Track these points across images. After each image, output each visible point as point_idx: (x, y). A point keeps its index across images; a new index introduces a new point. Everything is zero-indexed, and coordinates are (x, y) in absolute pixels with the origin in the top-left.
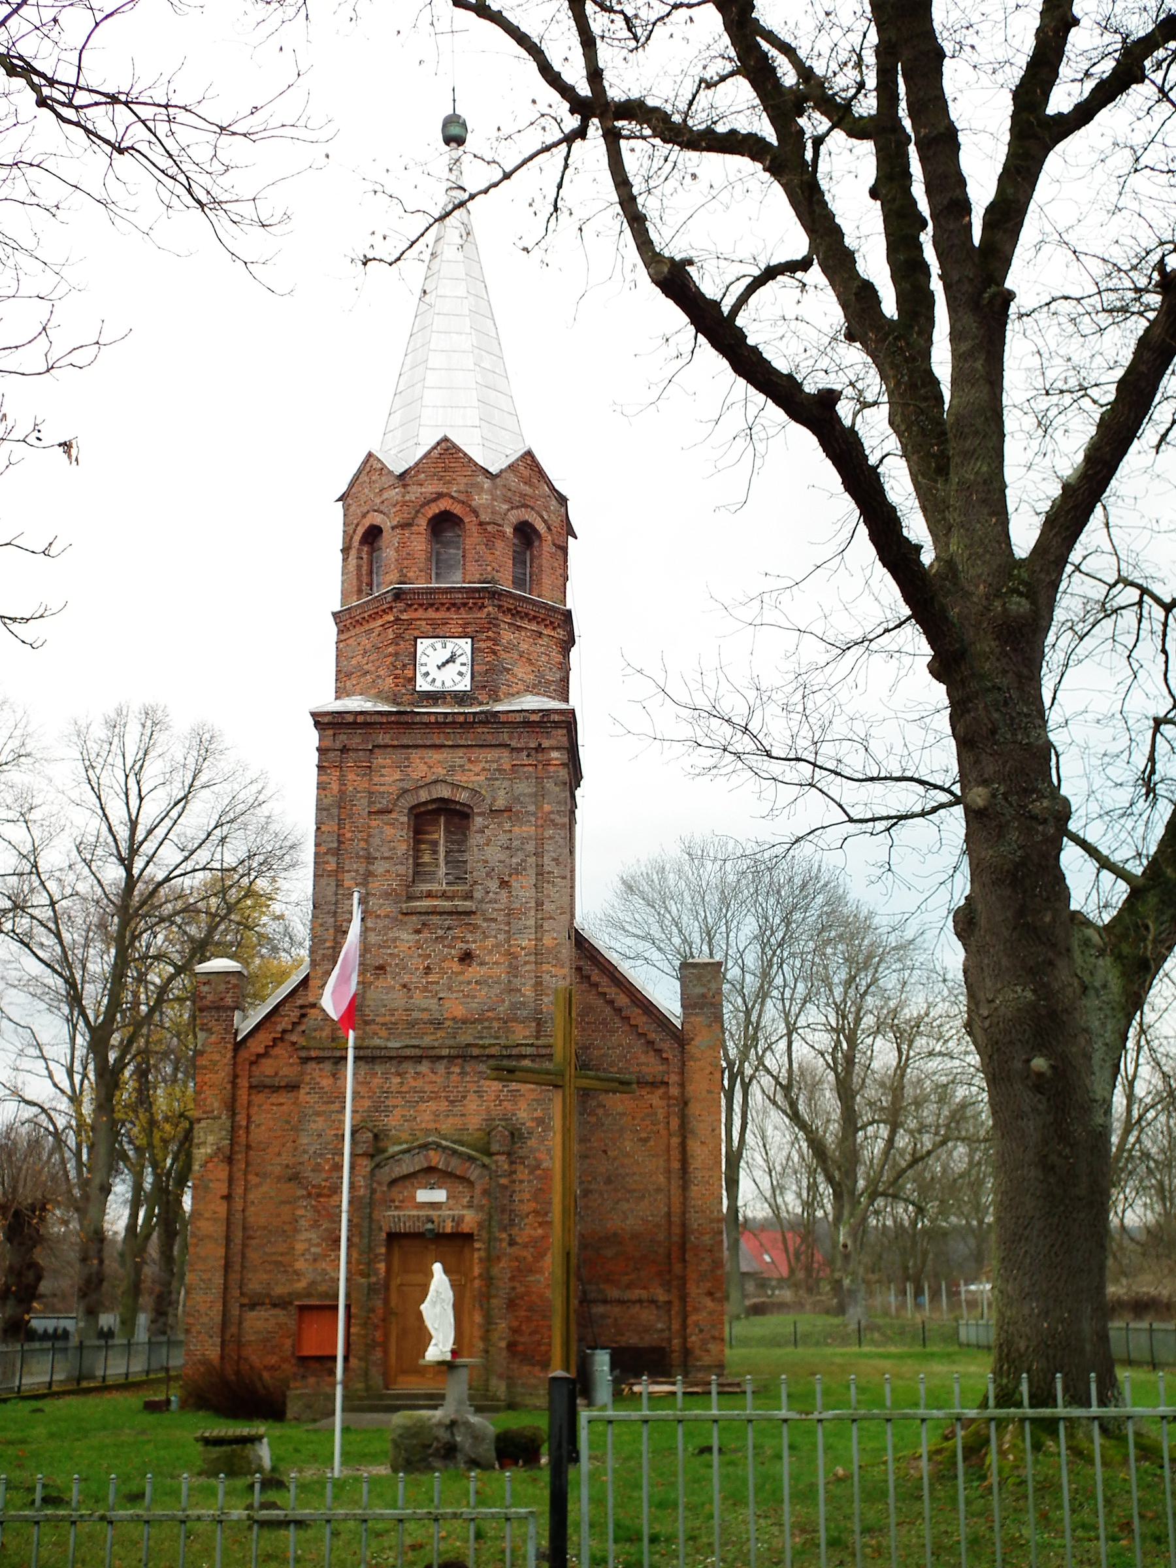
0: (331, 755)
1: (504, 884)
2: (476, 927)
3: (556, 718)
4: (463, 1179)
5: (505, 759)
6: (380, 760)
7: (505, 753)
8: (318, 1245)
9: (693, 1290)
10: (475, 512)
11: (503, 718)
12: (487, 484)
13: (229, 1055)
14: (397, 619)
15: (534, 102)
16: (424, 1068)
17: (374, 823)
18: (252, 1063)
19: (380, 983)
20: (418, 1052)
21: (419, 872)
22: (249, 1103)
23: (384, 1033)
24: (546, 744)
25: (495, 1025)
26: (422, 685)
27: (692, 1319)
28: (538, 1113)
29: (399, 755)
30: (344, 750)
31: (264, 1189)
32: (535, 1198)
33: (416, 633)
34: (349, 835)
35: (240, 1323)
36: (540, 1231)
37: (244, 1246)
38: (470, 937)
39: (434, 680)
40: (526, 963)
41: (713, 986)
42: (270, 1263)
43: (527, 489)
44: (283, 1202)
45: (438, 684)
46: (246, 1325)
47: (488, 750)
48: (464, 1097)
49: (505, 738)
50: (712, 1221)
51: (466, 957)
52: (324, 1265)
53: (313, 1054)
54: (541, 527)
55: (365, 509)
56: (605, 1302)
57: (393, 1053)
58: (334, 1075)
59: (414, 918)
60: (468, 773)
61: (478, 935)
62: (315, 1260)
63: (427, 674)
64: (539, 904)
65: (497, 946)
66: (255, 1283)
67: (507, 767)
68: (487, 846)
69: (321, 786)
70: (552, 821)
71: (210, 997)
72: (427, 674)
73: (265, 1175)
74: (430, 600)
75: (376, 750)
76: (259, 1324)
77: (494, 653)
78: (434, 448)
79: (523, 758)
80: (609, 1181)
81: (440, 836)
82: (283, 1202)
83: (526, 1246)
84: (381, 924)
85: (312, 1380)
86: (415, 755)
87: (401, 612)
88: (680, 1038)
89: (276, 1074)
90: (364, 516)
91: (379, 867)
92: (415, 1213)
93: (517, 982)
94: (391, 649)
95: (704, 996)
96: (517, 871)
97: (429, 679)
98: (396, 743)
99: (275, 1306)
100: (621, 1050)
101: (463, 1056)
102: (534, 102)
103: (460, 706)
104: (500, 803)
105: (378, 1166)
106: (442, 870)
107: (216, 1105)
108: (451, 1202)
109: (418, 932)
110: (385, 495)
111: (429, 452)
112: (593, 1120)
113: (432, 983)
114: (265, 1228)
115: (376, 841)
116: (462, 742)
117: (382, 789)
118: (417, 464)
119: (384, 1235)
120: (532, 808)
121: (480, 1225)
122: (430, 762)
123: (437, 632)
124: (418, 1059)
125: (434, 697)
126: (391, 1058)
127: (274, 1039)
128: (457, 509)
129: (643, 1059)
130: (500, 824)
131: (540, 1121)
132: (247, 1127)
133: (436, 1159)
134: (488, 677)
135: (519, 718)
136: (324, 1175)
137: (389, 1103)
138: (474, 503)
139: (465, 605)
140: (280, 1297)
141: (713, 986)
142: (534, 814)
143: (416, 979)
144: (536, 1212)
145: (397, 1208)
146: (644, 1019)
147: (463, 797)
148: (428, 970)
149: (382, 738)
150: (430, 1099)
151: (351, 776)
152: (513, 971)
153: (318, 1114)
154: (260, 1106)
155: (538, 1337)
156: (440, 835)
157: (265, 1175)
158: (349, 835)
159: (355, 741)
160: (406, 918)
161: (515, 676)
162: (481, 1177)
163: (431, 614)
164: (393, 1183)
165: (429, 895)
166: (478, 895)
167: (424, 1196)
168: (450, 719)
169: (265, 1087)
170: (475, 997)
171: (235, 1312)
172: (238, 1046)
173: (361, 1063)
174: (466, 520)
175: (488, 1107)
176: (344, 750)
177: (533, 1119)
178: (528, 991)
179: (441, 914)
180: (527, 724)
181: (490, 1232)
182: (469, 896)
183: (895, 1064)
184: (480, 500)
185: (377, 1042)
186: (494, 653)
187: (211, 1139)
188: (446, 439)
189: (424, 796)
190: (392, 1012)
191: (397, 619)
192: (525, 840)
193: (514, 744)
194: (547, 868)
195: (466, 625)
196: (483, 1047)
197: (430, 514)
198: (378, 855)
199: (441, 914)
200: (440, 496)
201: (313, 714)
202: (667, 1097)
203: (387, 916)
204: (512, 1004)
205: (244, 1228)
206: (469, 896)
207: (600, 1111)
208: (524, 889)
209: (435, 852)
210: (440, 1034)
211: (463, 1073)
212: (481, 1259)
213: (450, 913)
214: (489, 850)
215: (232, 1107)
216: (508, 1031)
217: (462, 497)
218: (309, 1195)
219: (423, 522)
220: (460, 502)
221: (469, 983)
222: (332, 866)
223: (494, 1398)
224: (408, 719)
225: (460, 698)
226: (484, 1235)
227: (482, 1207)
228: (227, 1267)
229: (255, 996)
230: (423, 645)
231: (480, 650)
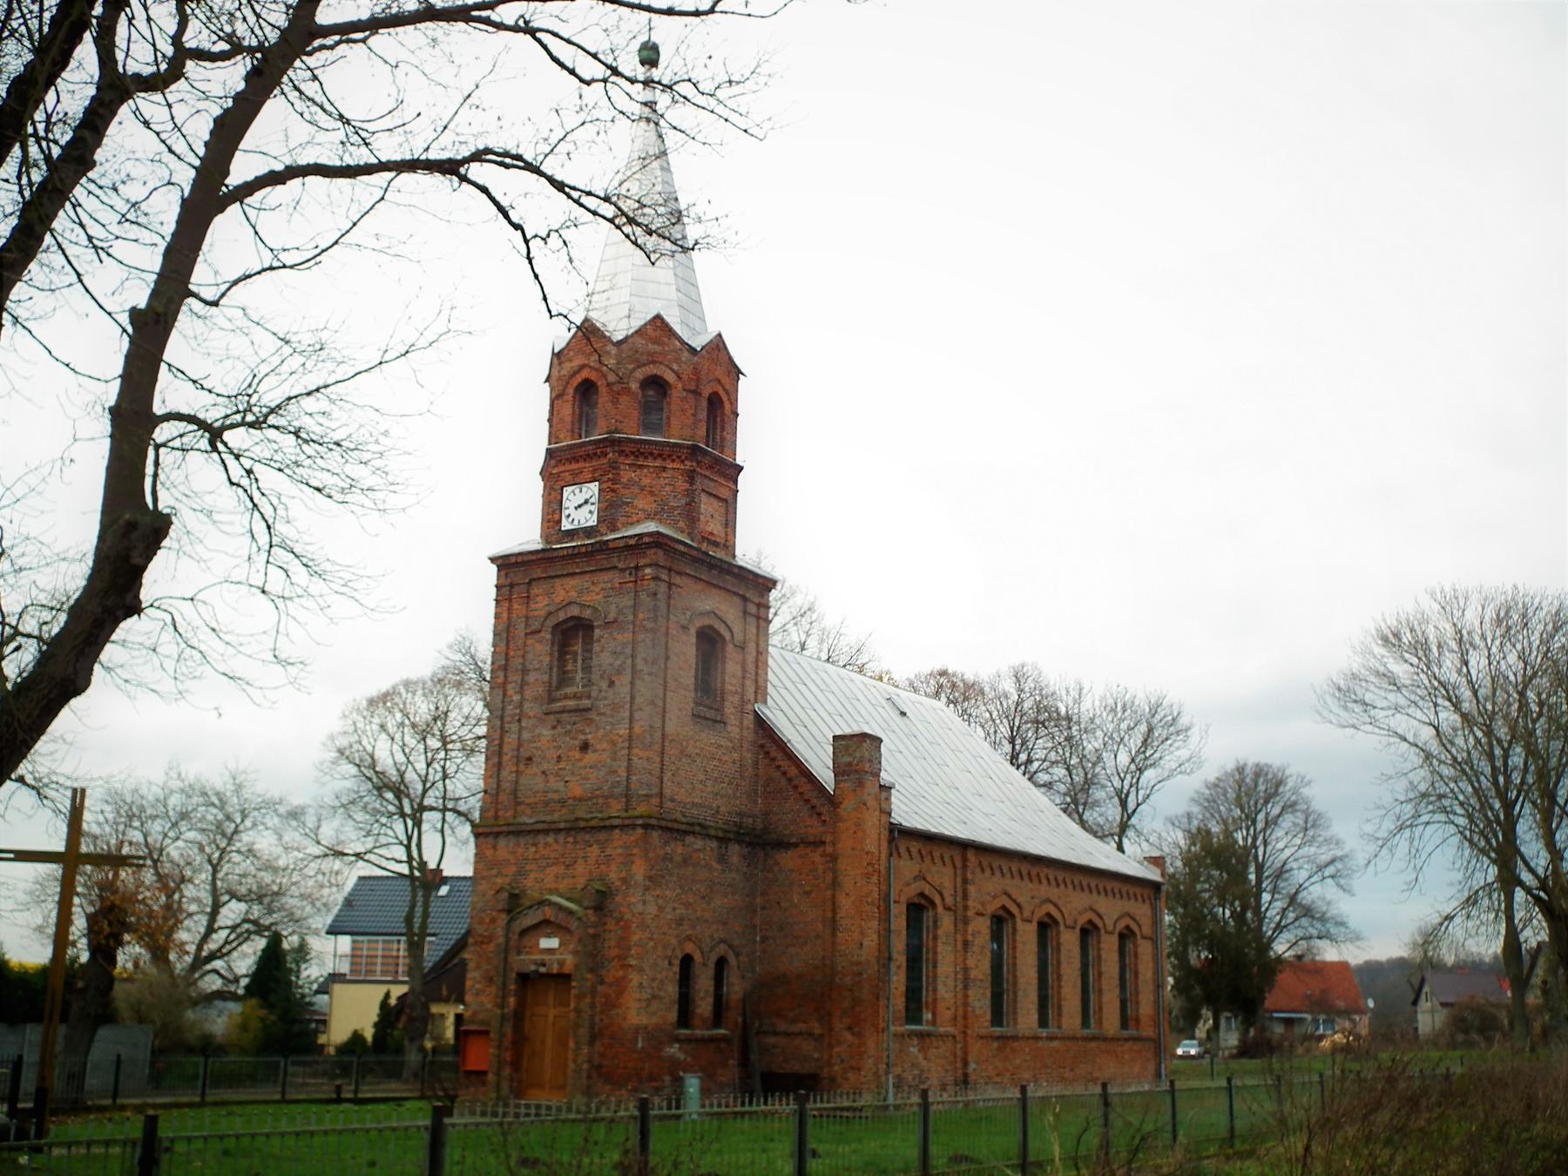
1: (611, 684)
2: (592, 720)
3: (646, 540)
4: (567, 930)
5: (616, 578)
9: (838, 1025)
11: (611, 545)
16: (550, 839)
19: (528, 771)
21: (564, 679)
23: (528, 812)
26: (566, 525)
28: (623, 874)
29: (546, 586)
30: (512, 586)
41: (858, 755)
43: (657, 348)
50: (853, 964)
51: (585, 747)
54: (670, 377)
56: (775, 1034)
64: (633, 698)
69: (497, 616)
80: (781, 929)
83: (610, 985)
84: (531, 722)
88: (833, 801)
91: (531, 677)
95: (850, 764)
100: (791, 817)
109: (554, 728)
112: (770, 875)
121: (576, 966)
124: (546, 832)
125: (571, 534)
129: (808, 823)
131: (624, 881)
134: (610, 511)
135: (621, 543)
144: (619, 957)
146: (809, 787)
147: (587, 614)
151: (516, 606)
156: (578, 648)
161: (634, 507)
163: (568, 467)
165: (566, 697)
173: (481, 839)
180: (628, 547)
183: (1118, 819)
186: (613, 491)
189: (562, 616)
193: (620, 565)
195: (595, 471)
201: (493, 560)
202: (824, 855)
207: (776, 869)
209: (575, 661)
210: (565, 810)
213: (575, 711)
216: (608, 806)
222: (501, 680)
225: (588, 532)
229: (239, 788)
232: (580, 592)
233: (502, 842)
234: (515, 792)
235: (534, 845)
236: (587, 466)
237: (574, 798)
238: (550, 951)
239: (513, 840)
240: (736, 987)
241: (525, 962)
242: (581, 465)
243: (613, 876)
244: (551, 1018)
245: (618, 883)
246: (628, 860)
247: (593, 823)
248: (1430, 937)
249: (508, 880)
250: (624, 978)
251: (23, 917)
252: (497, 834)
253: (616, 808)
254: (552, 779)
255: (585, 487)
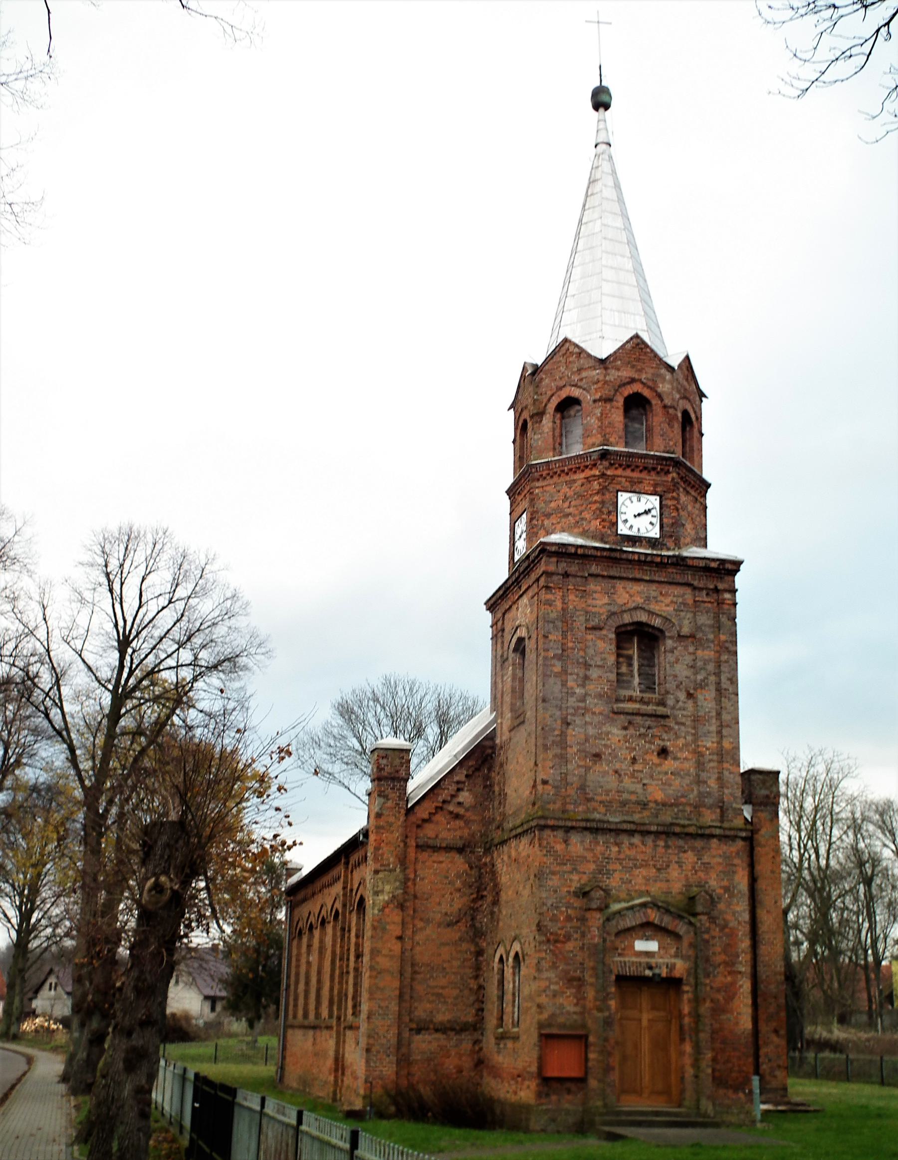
0: (555, 578)
1: (690, 696)
2: (671, 729)
4: (677, 936)
6: (592, 586)
7: (688, 591)
8: (557, 983)
10: (660, 396)
11: (690, 562)
12: (668, 377)
13: (402, 818)
14: (603, 475)
15: (601, 100)
16: (636, 840)
17: (589, 637)
18: (418, 826)
19: (597, 768)
20: (633, 827)
22: (416, 859)
23: (602, 809)
24: (721, 586)
25: (688, 809)
26: (623, 529)
27: (763, 1051)
28: (725, 883)
31: (428, 931)
32: (725, 951)
33: (618, 487)
34: (570, 645)
35: (409, 1045)
36: (729, 979)
37: (413, 979)
38: (665, 736)
39: (631, 527)
40: (710, 761)
42: (433, 994)
44: (443, 944)
45: (635, 530)
46: (413, 1046)
47: (674, 587)
48: (668, 866)
49: (689, 578)
51: (663, 752)
52: (561, 1000)
53: (550, 822)
55: (562, 383)
57: (613, 827)
58: (565, 841)
59: (622, 717)
60: (662, 604)
61: (671, 735)
62: (554, 996)
63: (626, 521)
64: (719, 714)
65: (686, 745)
66: (421, 1011)
67: (690, 602)
68: (676, 663)
70: (727, 648)
71: (388, 769)
72: (626, 521)
73: (428, 921)
74: (628, 462)
75: (590, 579)
76: (424, 1046)
77: (677, 509)
78: (627, 342)
79: (703, 596)
81: (634, 652)
82: (443, 944)
83: (718, 990)
84: (596, 719)
85: (554, 1098)
86: (620, 585)
87: (607, 469)
89: (437, 836)
90: (560, 388)
91: (594, 673)
92: (634, 959)
93: (704, 775)
94: (596, 498)
95: (767, 797)
96: (702, 685)
97: (628, 525)
98: (605, 573)
99: (437, 1030)
101: (667, 833)
102: (601, 100)
103: (653, 548)
104: (686, 630)
105: (608, 919)
106: (637, 680)
107: (391, 860)
108: (662, 952)
109: (625, 728)
110: (584, 374)
111: (624, 345)
113: (638, 771)
114: (428, 965)
115: (591, 651)
116: (657, 578)
117: (594, 610)
118: (615, 352)
119: (613, 977)
120: (711, 636)
122: (632, 591)
123: (635, 488)
124: (631, 833)
126: (610, 830)
127: (437, 808)
128: (646, 393)
130: (686, 648)
131: (727, 889)
132: (414, 880)
133: (653, 916)
135: (702, 564)
136: (559, 925)
137: (610, 867)
138: (659, 390)
139: (654, 469)
140: (441, 1023)
141: (774, 789)
142: (713, 642)
143: (624, 766)
144: (726, 963)
145: (620, 955)
147: (657, 622)
148: (634, 760)
149: (594, 569)
150: (641, 866)
152: (700, 765)
153: (553, 873)
154: (423, 862)
155: (730, 1065)
157: (428, 921)
158: (570, 645)
159: (573, 569)
160: (615, 717)
162: (688, 932)
163: (628, 473)
164: (618, 934)
165: (630, 699)
166: (670, 702)
167: (641, 945)
168: (649, 559)
169: (429, 847)
170: (670, 785)
171: (406, 1034)
172: (409, 811)
174: (653, 402)
175: (686, 876)
176: (566, 575)
177: (721, 887)
178: (713, 784)
179: (643, 715)
181: (696, 978)
182: (662, 703)
184: (664, 387)
185: (597, 816)
187: (387, 888)
188: (637, 336)
189: (627, 619)
190: (607, 792)
191: (603, 475)
192: (706, 662)
193: (696, 583)
194: (724, 686)
196: (684, 826)
197: (626, 394)
198: (592, 663)
199: (643, 715)
200: (632, 381)
203: (600, 713)
204: (700, 792)
205: (413, 965)
206: (662, 703)
208: (707, 699)
209: (630, 665)
210: (646, 813)
211: (667, 847)
212: (689, 1001)
214: (678, 667)
215: (403, 861)
216: (700, 814)
217: (650, 384)
218: (548, 941)
219: (620, 401)
220: (649, 387)
221: (666, 773)
223: (705, 1115)
224: (617, 555)
225: (652, 542)
226: (692, 981)
227: (689, 956)
228: (401, 996)
230: (623, 497)
231: (666, 506)
232: (648, 599)
233: (575, 838)
234: (582, 788)
235: (617, 844)
236: (649, 478)
237: (656, 802)
238: (648, 954)
239: (588, 838)
240: (272, 1008)
241: (620, 962)
242: (644, 475)
243: (714, 882)
244: (645, 1023)
245: (720, 891)
246: (729, 871)
247: (691, 830)
248: (68, 994)
249: (585, 879)
250: (733, 984)
251: (660, 850)
252: (568, 830)
253: (709, 817)
254: (626, 779)
255: (644, 498)
